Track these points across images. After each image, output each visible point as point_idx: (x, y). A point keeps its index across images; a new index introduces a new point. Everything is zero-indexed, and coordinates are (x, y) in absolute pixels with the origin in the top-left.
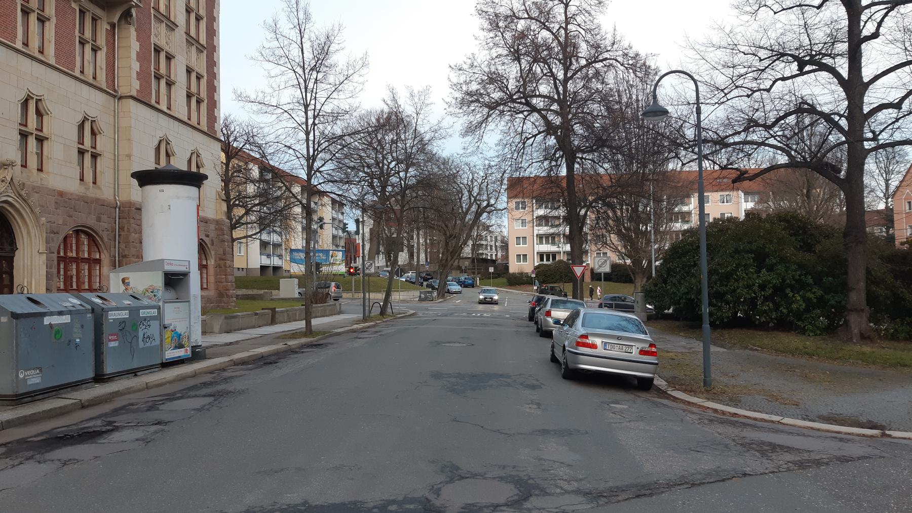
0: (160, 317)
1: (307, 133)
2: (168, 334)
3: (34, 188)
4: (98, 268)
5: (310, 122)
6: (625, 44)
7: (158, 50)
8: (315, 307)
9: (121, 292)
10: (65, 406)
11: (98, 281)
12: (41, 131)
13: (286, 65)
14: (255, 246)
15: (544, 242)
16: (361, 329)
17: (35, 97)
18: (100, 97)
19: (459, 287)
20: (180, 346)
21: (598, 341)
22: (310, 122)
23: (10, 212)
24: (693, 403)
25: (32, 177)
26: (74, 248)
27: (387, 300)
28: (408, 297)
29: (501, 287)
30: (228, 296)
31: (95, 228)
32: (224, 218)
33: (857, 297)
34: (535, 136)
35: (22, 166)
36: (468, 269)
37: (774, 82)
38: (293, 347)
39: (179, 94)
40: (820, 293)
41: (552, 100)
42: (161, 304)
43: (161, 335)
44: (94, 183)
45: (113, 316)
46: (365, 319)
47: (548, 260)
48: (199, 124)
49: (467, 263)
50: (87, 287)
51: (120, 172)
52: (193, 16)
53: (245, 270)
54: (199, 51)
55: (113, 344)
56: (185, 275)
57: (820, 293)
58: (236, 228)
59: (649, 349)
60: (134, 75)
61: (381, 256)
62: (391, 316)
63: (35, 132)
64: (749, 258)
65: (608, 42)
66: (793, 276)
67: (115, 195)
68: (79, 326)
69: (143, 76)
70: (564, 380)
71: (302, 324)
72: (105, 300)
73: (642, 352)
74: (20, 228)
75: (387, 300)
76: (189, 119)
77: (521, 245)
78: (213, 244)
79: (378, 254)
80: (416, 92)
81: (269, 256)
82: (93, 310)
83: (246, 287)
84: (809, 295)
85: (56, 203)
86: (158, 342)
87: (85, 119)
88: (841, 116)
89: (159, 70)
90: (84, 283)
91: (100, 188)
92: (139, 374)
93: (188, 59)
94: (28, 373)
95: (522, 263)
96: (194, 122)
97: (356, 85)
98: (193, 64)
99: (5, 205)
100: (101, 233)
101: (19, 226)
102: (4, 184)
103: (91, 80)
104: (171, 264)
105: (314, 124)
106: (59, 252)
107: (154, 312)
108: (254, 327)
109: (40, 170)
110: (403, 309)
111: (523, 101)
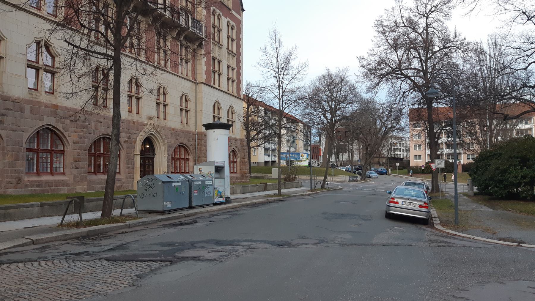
0: (213, 184)
1: (279, 100)
2: (216, 192)
3: (162, 127)
4: (188, 163)
5: (281, 95)
6: (462, 37)
7: (214, 59)
8: (287, 183)
9: (199, 174)
10: (180, 216)
11: (188, 168)
12: (165, 101)
13: (270, 68)
14: (262, 150)
16: (308, 194)
17: (162, 87)
18: (189, 84)
19: (377, 175)
20: (221, 197)
21: (399, 201)
22: (281, 95)
23: (152, 138)
24: (439, 230)
25: (162, 122)
26: (178, 153)
27: (325, 180)
28: (343, 180)
29: (404, 175)
30: (246, 177)
31: (187, 144)
32: (244, 138)
34: (409, 91)
35: (157, 118)
36: (385, 164)
38: (270, 201)
39: (224, 78)
41: (419, 71)
42: (213, 179)
43: (213, 192)
44: (187, 124)
45: (196, 183)
46: (311, 190)
48: (233, 92)
49: (384, 160)
50: (183, 171)
51: (198, 118)
52: (230, 39)
53: (257, 163)
54: (233, 56)
55: (195, 194)
56: (223, 167)
58: (252, 141)
59: (424, 205)
60: (204, 72)
61: (333, 156)
62: (327, 189)
63: (163, 102)
64: (517, 161)
65: (452, 37)
67: (195, 129)
68: (184, 187)
69: (208, 73)
70: (386, 219)
71: (276, 192)
72: (193, 177)
73: (420, 206)
74: (157, 145)
75: (325, 180)
76: (228, 90)
78: (239, 151)
79: (332, 154)
80: (341, 70)
81: (269, 156)
82: (189, 181)
83: (257, 172)
85: (171, 133)
86: (212, 195)
87: (183, 95)
89: (214, 69)
90: (182, 169)
91: (189, 126)
92: (205, 207)
93: (228, 61)
94: (167, 203)
95: (418, 160)
96: (230, 92)
97: (302, 75)
98: (230, 64)
99: (151, 135)
100: (189, 147)
101: (155, 141)
102: (151, 126)
103: (185, 77)
104: (218, 163)
105: (282, 96)
106: (172, 156)
107: (211, 182)
108: (256, 192)
109: (165, 119)
110: (337, 186)
111: (399, 72)
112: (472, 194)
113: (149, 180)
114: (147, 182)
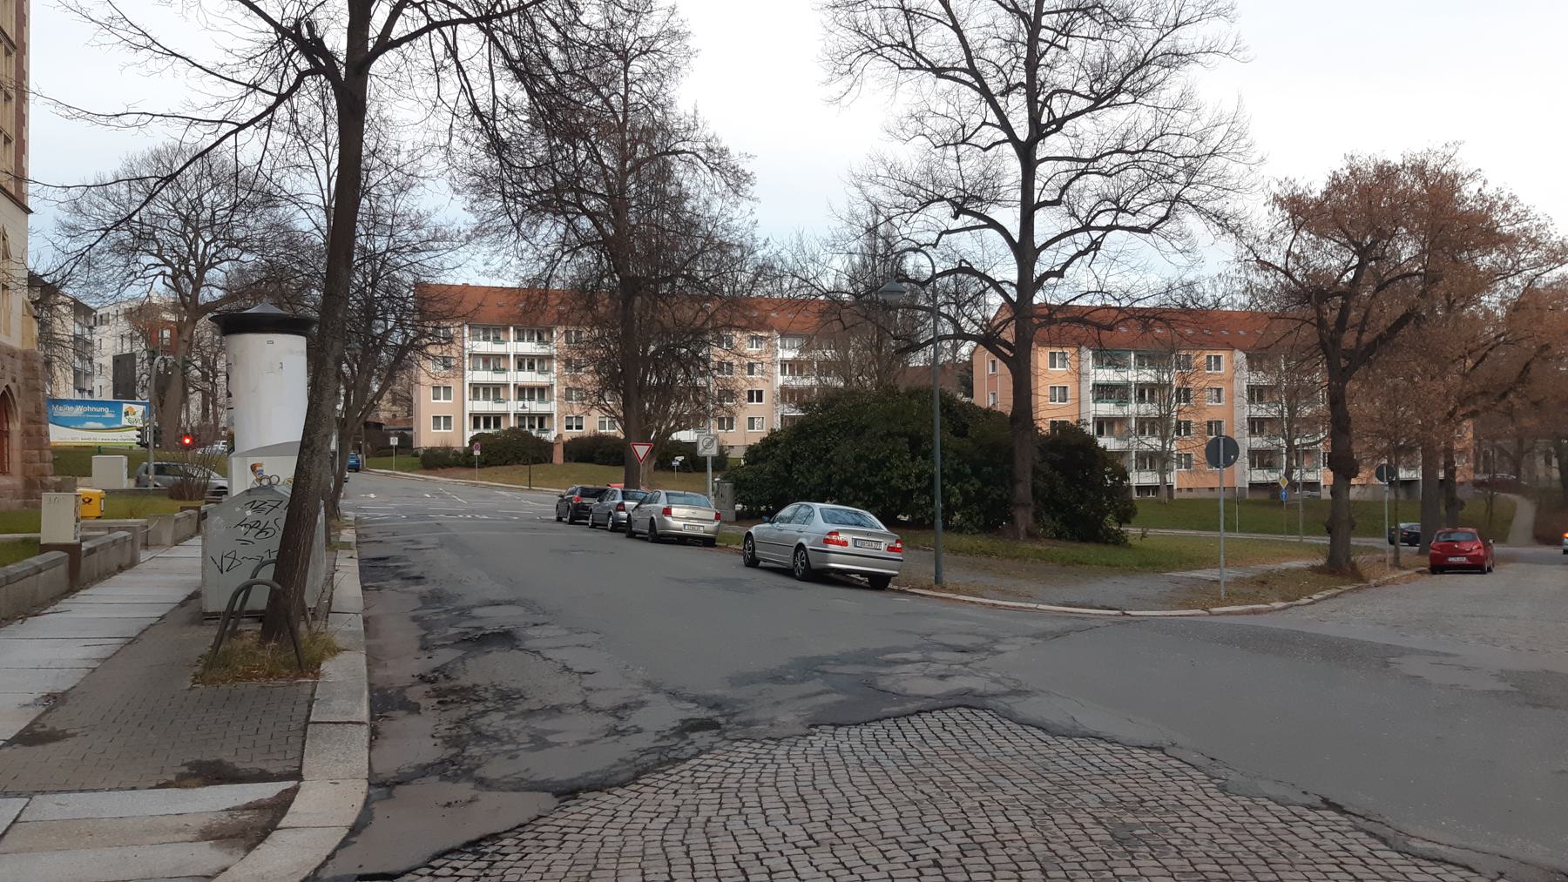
15: (481, 396)
29: (409, 472)
33: (1023, 490)
37: (940, 236)
40: (978, 485)
47: (487, 426)
57: (978, 485)
64: (903, 444)
66: (951, 465)
73: (890, 549)
77: (442, 401)
84: (967, 486)
88: (1011, 284)
95: (442, 430)
112: (733, 517)
113: (257, 509)
114: (249, 513)
